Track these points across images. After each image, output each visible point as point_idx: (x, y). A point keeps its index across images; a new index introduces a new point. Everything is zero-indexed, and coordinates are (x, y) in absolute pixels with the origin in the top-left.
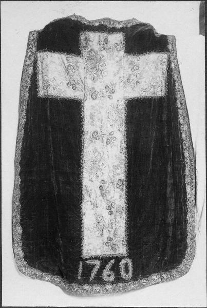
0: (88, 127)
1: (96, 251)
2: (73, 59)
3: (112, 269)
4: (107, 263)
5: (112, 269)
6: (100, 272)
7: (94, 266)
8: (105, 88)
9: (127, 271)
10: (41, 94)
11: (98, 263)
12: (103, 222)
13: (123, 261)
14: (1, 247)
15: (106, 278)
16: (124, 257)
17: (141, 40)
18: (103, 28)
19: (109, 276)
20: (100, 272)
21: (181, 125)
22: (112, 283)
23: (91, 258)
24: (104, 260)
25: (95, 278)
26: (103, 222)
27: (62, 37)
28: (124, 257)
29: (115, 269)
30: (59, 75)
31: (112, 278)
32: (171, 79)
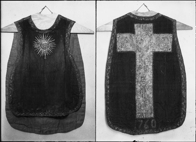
8: (146, 45)
9: (154, 125)
17: (164, 25)
24: (144, 120)
30: (126, 43)
32: (175, 44)
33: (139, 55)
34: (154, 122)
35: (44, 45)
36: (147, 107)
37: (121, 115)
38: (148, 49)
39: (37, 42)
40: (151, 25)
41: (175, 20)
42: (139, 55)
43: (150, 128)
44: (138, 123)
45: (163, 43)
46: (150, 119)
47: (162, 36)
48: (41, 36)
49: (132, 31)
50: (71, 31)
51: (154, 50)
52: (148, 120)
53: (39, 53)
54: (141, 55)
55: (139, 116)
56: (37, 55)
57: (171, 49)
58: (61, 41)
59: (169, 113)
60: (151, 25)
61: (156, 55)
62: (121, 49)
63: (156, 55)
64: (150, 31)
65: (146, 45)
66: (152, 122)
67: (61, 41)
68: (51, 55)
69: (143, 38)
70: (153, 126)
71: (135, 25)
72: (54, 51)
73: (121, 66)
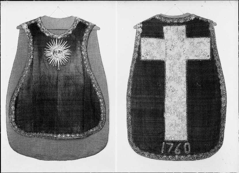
0: (168, 74)
1: (171, 138)
2: (161, 40)
3: (179, 148)
4: (177, 145)
5: (179, 148)
6: (173, 149)
7: (170, 146)
8: (176, 52)
9: (187, 150)
10: (143, 58)
11: (172, 144)
12: (176, 124)
13: (186, 144)
14: (238, 38)
15: (176, 152)
16: (186, 142)
17: (198, 28)
18: (174, 22)
19: (178, 151)
20: (173, 149)
21: (35, 22)
22: (179, 155)
23: (168, 142)
24: (175, 143)
25: (171, 152)
26: (176, 124)
27: (153, 28)
28: (186, 142)
29: (181, 149)
30: (152, 50)
31: (179, 152)
32: (213, 50)
33: (170, 65)
34: (187, 146)
35: (58, 53)
36: (179, 127)
37: (148, 137)
38: (181, 56)
39: (48, 48)
40: (183, 28)
41: (212, 22)
42: (170, 65)
43: (183, 153)
44: (167, 147)
45: (199, 49)
46: (183, 142)
47: (196, 40)
48: (53, 42)
49: (159, 35)
50: (166, 133)
51: (187, 58)
52: (180, 144)
53: (52, 62)
54: (172, 64)
55: (168, 138)
56: (49, 65)
57: (209, 56)
58: (79, 48)
59: (205, 136)
60: (183, 28)
61: (191, 64)
62: (205, 41)
63: (191, 64)
64: (183, 35)
65: (176, 52)
66: (185, 146)
67: (79, 48)
68: (64, 65)
69: (173, 44)
70: (186, 152)
71: (165, 28)
72: (70, 58)
73: (148, 77)
